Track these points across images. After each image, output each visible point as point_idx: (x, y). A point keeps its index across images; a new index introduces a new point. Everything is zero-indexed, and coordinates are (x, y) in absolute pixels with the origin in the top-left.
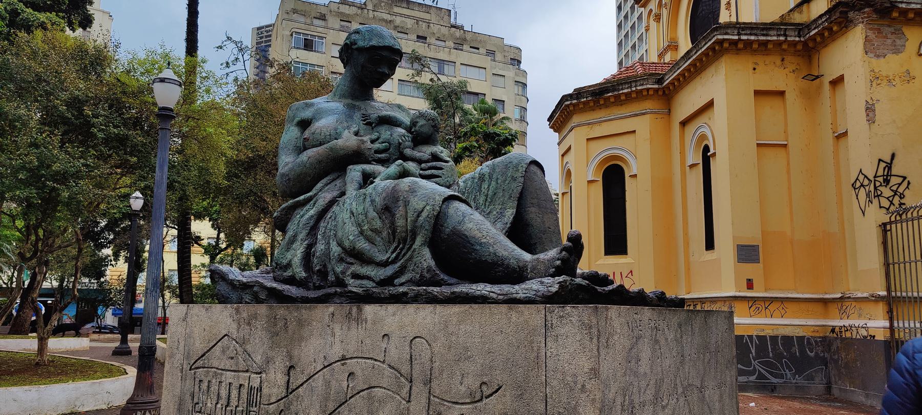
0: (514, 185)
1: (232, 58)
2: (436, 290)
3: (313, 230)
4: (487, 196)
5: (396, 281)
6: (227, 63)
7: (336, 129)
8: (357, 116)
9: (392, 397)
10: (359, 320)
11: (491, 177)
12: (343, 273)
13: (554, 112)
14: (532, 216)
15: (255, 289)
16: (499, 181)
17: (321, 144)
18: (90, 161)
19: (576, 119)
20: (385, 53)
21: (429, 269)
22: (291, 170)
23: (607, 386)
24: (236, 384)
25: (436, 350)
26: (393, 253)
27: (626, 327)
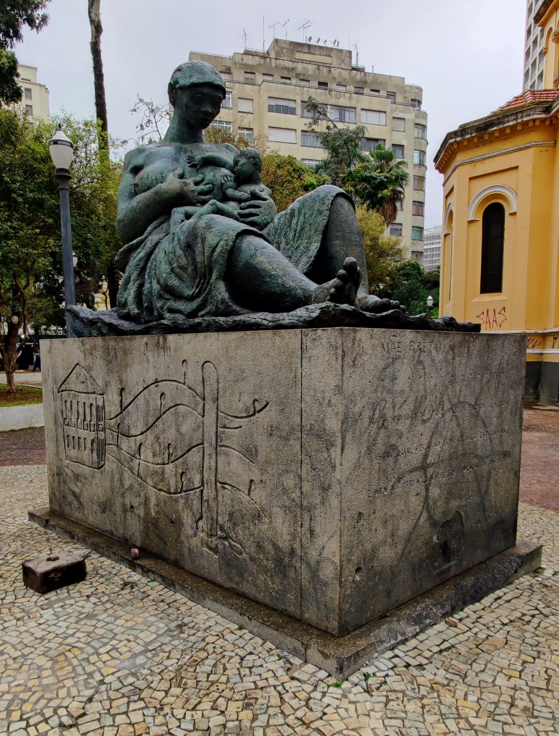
0: (320, 218)
1: (145, 120)
2: (221, 319)
3: (143, 270)
4: (295, 231)
5: (200, 314)
6: (142, 126)
7: (161, 173)
8: (183, 158)
9: (191, 413)
10: (165, 348)
11: (300, 213)
12: (162, 308)
13: (439, 152)
14: (337, 248)
15: (99, 324)
16: (307, 216)
17: (149, 188)
18: (15, 224)
19: (460, 158)
20: (206, 90)
21: (223, 301)
22: (125, 215)
23: (353, 401)
24: (88, 404)
25: (220, 372)
26: (197, 288)
27: (380, 349)
